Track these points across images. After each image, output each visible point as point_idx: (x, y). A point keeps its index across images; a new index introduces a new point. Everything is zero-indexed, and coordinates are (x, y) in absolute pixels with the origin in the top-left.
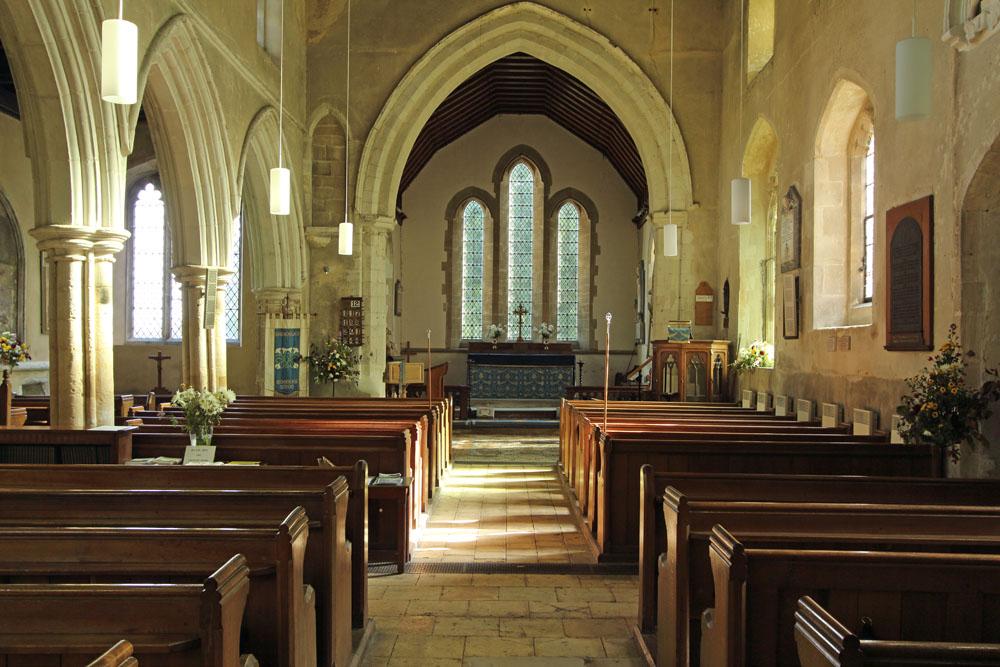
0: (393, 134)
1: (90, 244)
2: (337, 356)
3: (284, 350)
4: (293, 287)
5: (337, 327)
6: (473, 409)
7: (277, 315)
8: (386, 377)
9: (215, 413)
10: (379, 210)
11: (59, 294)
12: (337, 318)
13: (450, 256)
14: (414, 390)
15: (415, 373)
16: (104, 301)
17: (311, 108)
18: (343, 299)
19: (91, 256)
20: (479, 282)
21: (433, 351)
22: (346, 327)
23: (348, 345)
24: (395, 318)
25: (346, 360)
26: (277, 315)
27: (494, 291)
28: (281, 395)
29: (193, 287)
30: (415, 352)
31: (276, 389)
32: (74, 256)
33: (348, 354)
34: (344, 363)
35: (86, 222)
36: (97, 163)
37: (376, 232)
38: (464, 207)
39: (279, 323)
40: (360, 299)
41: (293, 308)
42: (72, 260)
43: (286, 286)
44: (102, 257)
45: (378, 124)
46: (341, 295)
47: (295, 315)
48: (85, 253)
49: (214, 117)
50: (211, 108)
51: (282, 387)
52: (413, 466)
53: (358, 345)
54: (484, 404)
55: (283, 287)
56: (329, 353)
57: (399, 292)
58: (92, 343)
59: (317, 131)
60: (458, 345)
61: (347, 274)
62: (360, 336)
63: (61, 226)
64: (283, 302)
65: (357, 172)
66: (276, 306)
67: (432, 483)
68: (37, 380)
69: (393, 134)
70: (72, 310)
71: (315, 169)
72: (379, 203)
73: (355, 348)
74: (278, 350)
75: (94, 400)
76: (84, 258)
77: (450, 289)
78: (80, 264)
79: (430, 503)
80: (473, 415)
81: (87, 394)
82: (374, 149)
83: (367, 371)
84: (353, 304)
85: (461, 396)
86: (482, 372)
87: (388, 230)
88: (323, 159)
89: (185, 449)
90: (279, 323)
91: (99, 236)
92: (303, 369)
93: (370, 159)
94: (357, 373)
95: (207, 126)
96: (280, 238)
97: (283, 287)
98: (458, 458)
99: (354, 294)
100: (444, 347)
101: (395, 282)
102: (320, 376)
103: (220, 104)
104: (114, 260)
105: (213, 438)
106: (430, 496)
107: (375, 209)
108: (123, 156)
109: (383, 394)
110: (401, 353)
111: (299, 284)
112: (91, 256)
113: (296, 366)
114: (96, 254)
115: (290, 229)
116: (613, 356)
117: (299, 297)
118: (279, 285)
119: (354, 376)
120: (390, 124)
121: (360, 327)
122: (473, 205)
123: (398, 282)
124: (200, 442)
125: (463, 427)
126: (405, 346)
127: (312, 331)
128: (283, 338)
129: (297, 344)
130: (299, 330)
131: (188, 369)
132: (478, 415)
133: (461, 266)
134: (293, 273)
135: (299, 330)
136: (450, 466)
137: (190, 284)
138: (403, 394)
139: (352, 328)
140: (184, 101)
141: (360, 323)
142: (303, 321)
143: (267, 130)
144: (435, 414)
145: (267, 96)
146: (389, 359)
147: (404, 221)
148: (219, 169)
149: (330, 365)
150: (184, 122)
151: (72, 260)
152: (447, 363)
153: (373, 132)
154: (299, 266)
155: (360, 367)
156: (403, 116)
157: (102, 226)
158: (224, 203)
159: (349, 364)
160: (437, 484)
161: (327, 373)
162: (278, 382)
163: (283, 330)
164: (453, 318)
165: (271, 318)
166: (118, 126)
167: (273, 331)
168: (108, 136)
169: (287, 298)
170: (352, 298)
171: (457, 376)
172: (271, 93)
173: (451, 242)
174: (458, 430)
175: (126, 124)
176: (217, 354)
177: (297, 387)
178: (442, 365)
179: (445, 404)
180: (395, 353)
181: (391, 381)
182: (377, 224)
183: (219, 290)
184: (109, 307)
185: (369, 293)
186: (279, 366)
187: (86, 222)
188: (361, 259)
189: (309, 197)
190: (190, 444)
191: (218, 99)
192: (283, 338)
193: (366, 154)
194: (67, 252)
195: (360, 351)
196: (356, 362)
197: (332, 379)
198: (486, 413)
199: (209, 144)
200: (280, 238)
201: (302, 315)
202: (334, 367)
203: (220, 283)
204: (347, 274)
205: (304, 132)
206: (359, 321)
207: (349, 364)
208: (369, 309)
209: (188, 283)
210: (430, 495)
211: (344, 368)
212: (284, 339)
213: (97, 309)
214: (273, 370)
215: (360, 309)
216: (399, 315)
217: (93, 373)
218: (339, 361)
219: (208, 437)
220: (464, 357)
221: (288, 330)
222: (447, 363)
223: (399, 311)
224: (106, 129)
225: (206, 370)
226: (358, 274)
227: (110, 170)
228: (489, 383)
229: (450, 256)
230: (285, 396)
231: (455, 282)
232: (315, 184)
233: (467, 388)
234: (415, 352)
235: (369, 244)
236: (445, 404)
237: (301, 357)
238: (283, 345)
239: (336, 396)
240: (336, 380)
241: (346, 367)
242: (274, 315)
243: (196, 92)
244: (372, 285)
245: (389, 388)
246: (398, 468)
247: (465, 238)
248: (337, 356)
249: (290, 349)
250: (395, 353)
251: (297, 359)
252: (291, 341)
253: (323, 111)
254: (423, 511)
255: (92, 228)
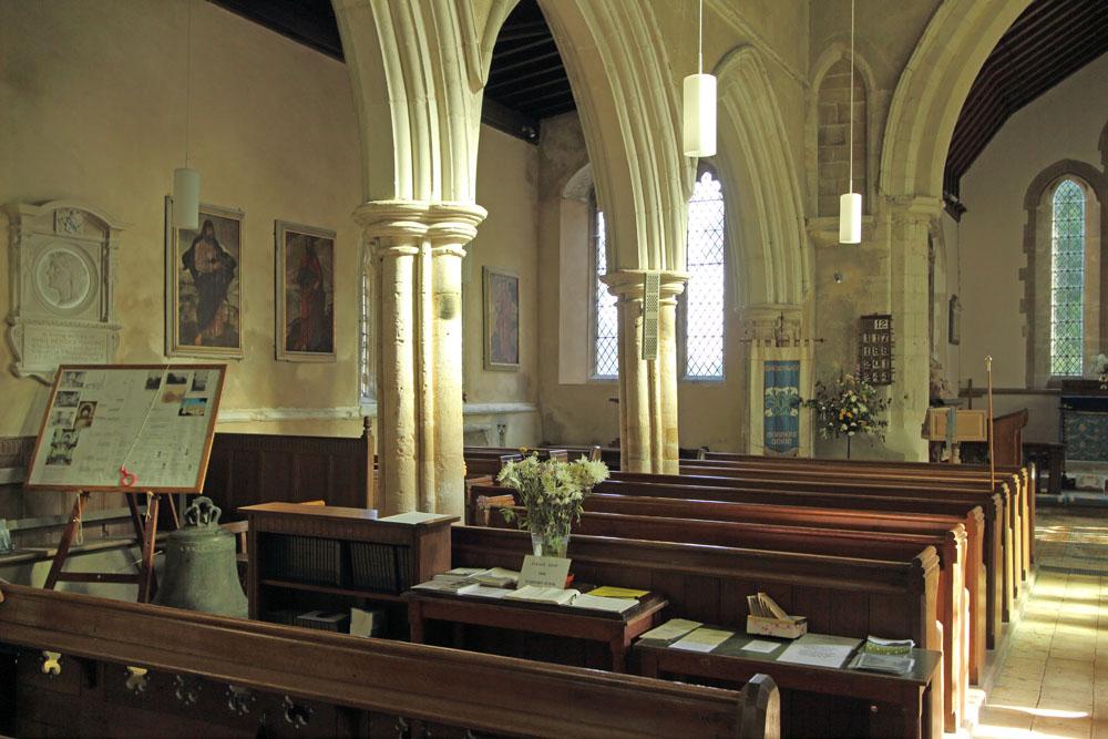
0: (936, 76)
1: (423, 229)
2: (853, 399)
3: (778, 390)
4: (790, 302)
5: (855, 358)
6: (1069, 475)
7: (768, 342)
8: (925, 432)
9: (567, 500)
10: (916, 186)
11: (385, 306)
12: (855, 346)
13: (1031, 259)
14: (973, 452)
15: (973, 425)
16: (446, 314)
17: (815, 54)
18: (863, 318)
19: (427, 247)
20: (1077, 299)
21: (995, 392)
22: (867, 358)
23: (871, 383)
24: (950, 347)
25: (867, 404)
26: (768, 342)
27: (1101, 306)
28: (775, 454)
29: (630, 300)
30: (980, 393)
31: (766, 444)
32: (401, 248)
33: (869, 396)
34: (864, 409)
35: (416, 195)
36: (660, 204)
37: (911, 219)
38: (1053, 188)
39: (770, 353)
40: (888, 317)
41: (790, 332)
42: (399, 254)
43: (781, 301)
44: (443, 248)
45: (914, 63)
46: (859, 313)
47: (792, 341)
48: (418, 242)
49: (651, 51)
50: (646, 39)
51: (774, 442)
52: (946, 615)
53: (886, 384)
54: (1087, 469)
55: (776, 302)
56: (841, 394)
57: (955, 311)
58: (428, 379)
59: (826, 84)
60: (1045, 384)
61: (869, 282)
62: (889, 371)
63: (379, 202)
64: (777, 324)
65: (882, 135)
66: (767, 331)
67: (993, 614)
68: (478, 426)
69: (936, 76)
70: (399, 330)
71: (822, 138)
72: (917, 178)
73: (881, 387)
74: (769, 391)
75: (431, 466)
76: (416, 250)
77: (1033, 305)
78: (410, 259)
79: (989, 660)
80: (1070, 485)
81: (421, 456)
82: (908, 99)
83: (900, 421)
84: (878, 325)
85: (1047, 457)
86: (1083, 423)
87: (931, 215)
88: (834, 122)
89: (523, 558)
90: (770, 353)
91: (435, 214)
92: (805, 416)
93: (903, 113)
94: (884, 424)
95: (642, 66)
96: (771, 235)
97: (776, 302)
98: (1048, 562)
99: (880, 311)
100: (1023, 386)
101: (950, 298)
102: (829, 428)
103: (659, 33)
104: (464, 253)
105: (573, 542)
106: (990, 643)
107: (910, 187)
108: (474, 91)
109: (924, 458)
110: (959, 395)
111: (798, 299)
112: (427, 247)
113: (794, 412)
114: (434, 244)
115: (784, 223)
116: (997, 397)
117: (799, 316)
118: (770, 299)
119: (879, 427)
120: (930, 61)
121: (889, 357)
122: (1068, 186)
123: (954, 298)
124: (549, 551)
125: (1053, 504)
126: (965, 385)
127: (817, 360)
128: (776, 374)
129: (795, 382)
130: (798, 362)
131: (625, 416)
132: (1078, 485)
133: (1049, 273)
134: (790, 282)
135: (798, 362)
136: (1030, 578)
137: (626, 297)
138: (951, 455)
139: (876, 358)
140: (605, 31)
141: (889, 352)
142: (804, 349)
143: (746, 81)
144: (1017, 481)
145: (744, 31)
146: (936, 402)
147: (963, 216)
148: (662, 129)
149: (843, 411)
150: (607, 61)
151: (399, 254)
152: (1026, 409)
153: (907, 76)
154: (798, 269)
155: (889, 415)
156: (954, 46)
157: (442, 199)
158: (670, 178)
159: (872, 411)
160: (1006, 617)
161: (838, 422)
162: (770, 434)
163: (776, 363)
164: (1037, 346)
165: (758, 346)
166: (464, 45)
167: (762, 363)
168: (446, 61)
169: (782, 318)
170: (876, 317)
171: (1044, 425)
172: (751, 28)
173: (1033, 240)
174: (1046, 509)
175: (476, 42)
176: (663, 397)
177: (795, 443)
178: (1019, 413)
179: (1021, 477)
180: (950, 393)
181: (934, 437)
182: (912, 209)
183: (665, 304)
184: (455, 325)
185: (903, 309)
186: (770, 413)
187: (416, 195)
188: (889, 259)
189: (813, 178)
190: (531, 552)
191: (655, 24)
192: (776, 374)
193: (896, 108)
194: (394, 241)
195: (889, 391)
196: (883, 408)
197: (847, 432)
198: (1091, 483)
199: (646, 94)
200: (771, 235)
201: (802, 341)
202: (849, 415)
203: (665, 294)
204: (869, 282)
205: (805, 87)
206: (887, 349)
207: (872, 411)
208: (902, 332)
209: (623, 295)
210: (990, 643)
211: (865, 416)
212: (777, 375)
213: (436, 327)
214: (762, 417)
215: (888, 332)
216: (957, 343)
217: (430, 423)
218: (856, 406)
219: (561, 542)
220: (1056, 400)
221: (783, 363)
222: (1026, 409)
223: (955, 338)
224: (443, 50)
225: (648, 418)
226: (886, 281)
227: (451, 114)
228: (1095, 438)
229: (1031, 259)
230: (780, 455)
231: (1039, 296)
232: (822, 158)
233: (1059, 448)
234: (980, 393)
235: (902, 239)
236: (1021, 477)
237: (801, 400)
238: (776, 384)
239: (853, 458)
240: (851, 433)
241: (866, 414)
242: (762, 342)
243: (623, 17)
244: (906, 296)
245: (935, 447)
246: (908, 625)
247: (1054, 234)
248: (853, 399)
249: (786, 389)
250: (950, 393)
251: (796, 403)
252: (787, 377)
253: (833, 56)
254: (974, 683)
255: (423, 205)
